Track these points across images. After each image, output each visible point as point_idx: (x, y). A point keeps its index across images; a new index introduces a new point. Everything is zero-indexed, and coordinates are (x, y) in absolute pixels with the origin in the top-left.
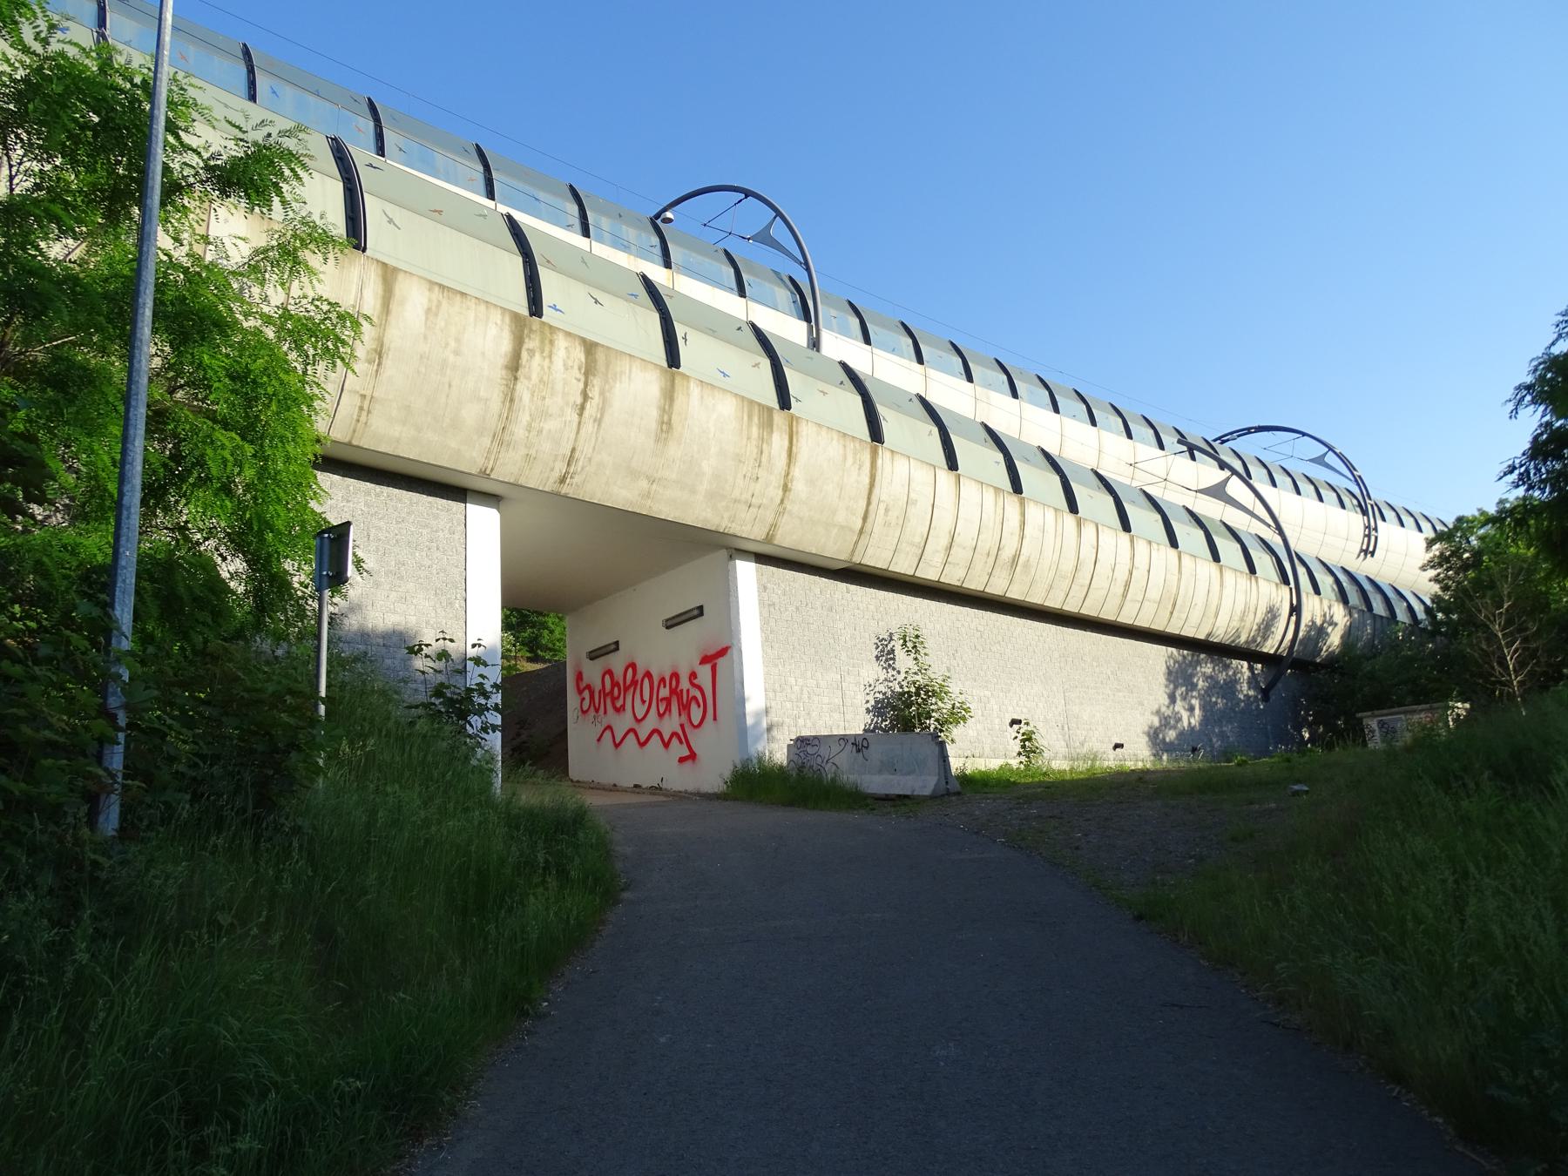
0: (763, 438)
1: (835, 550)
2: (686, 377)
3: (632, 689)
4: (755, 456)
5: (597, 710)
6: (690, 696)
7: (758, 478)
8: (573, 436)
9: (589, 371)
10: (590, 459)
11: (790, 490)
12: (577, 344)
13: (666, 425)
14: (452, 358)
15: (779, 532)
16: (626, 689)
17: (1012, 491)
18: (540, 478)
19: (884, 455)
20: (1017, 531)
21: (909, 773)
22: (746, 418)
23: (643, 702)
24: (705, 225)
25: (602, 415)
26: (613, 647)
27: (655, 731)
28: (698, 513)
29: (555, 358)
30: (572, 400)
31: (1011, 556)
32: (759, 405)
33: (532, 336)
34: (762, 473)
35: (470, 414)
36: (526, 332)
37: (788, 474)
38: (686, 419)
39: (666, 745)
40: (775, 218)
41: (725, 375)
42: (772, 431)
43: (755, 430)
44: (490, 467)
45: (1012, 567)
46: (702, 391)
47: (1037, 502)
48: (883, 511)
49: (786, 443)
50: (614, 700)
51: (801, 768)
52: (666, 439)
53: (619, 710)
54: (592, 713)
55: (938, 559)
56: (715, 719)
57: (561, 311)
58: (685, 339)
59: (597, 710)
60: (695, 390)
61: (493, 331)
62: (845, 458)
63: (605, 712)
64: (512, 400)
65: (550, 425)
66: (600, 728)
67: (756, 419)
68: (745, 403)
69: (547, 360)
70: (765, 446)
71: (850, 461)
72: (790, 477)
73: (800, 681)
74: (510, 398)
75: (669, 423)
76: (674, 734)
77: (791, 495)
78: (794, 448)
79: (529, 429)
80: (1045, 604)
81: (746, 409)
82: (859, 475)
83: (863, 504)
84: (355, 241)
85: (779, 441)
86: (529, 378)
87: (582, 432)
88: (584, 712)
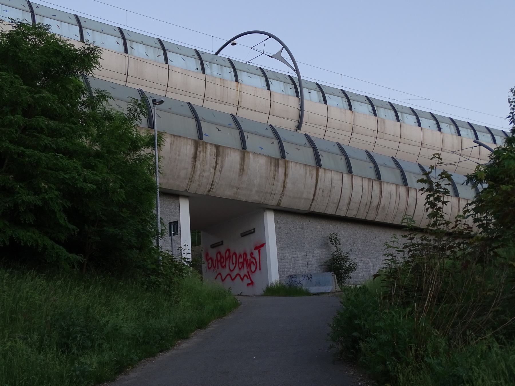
0: (275, 170)
1: (303, 206)
2: (249, 152)
3: (229, 259)
4: (272, 176)
5: (215, 267)
6: (251, 261)
7: (274, 184)
8: (213, 177)
9: (217, 155)
10: (218, 184)
11: (286, 187)
12: (213, 146)
13: (242, 170)
14: (177, 157)
15: (282, 202)
16: (226, 259)
17: (377, 179)
18: (203, 191)
19: (321, 171)
20: (379, 195)
21: (324, 286)
22: (269, 164)
23: (233, 264)
24: (251, 48)
25: (222, 169)
26: (221, 243)
27: (238, 275)
28: (255, 198)
29: (207, 153)
30: (212, 165)
31: (376, 205)
32: (274, 158)
33: (200, 147)
34: (275, 183)
35: (183, 174)
36: (198, 146)
37: (285, 182)
38: (249, 167)
39: (242, 279)
40: (283, 48)
41: (262, 149)
42: (279, 167)
43: (272, 168)
44: (188, 189)
45: (377, 209)
46: (254, 157)
47: (387, 183)
48: (322, 192)
49: (284, 171)
50: (221, 263)
51: (290, 286)
52: (242, 175)
53: (224, 267)
54: (213, 268)
55: (345, 208)
56: (260, 269)
57: (208, 136)
58: (248, 137)
59: (215, 267)
60: (251, 156)
61: (189, 147)
62: (306, 173)
63: (218, 268)
64: (195, 168)
65: (206, 174)
66: (216, 274)
67: (273, 164)
68: (269, 158)
69: (205, 154)
70: (276, 173)
71: (308, 174)
72: (285, 183)
73: (291, 255)
74: (194, 167)
75: (243, 169)
76: (245, 275)
77: (286, 189)
78: (287, 172)
79: (200, 176)
80: (393, 223)
81: (269, 161)
82: (311, 179)
83: (313, 190)
84: (160, 135)
85: (281, 170)
86: (199, 160)
87: (216, 175)
88: (209, 268)
